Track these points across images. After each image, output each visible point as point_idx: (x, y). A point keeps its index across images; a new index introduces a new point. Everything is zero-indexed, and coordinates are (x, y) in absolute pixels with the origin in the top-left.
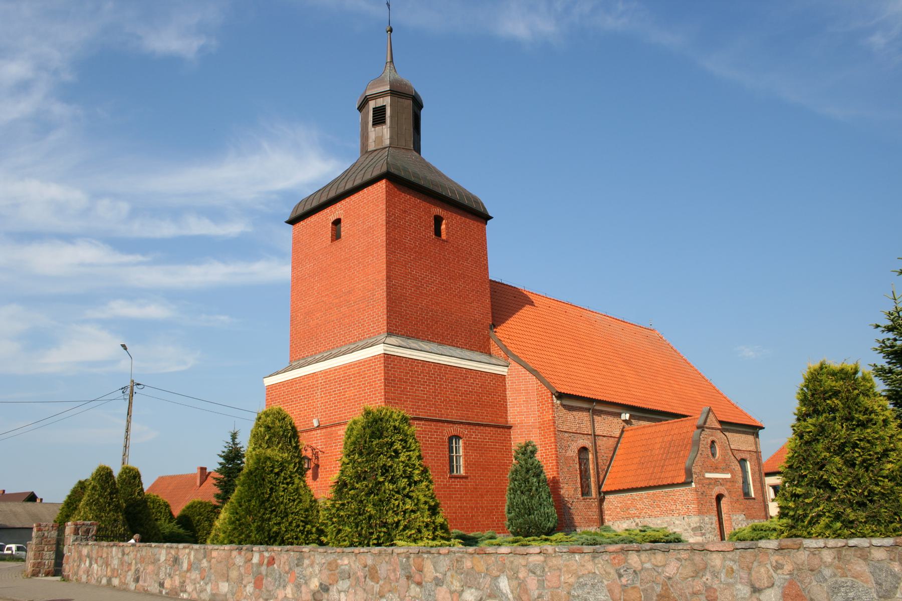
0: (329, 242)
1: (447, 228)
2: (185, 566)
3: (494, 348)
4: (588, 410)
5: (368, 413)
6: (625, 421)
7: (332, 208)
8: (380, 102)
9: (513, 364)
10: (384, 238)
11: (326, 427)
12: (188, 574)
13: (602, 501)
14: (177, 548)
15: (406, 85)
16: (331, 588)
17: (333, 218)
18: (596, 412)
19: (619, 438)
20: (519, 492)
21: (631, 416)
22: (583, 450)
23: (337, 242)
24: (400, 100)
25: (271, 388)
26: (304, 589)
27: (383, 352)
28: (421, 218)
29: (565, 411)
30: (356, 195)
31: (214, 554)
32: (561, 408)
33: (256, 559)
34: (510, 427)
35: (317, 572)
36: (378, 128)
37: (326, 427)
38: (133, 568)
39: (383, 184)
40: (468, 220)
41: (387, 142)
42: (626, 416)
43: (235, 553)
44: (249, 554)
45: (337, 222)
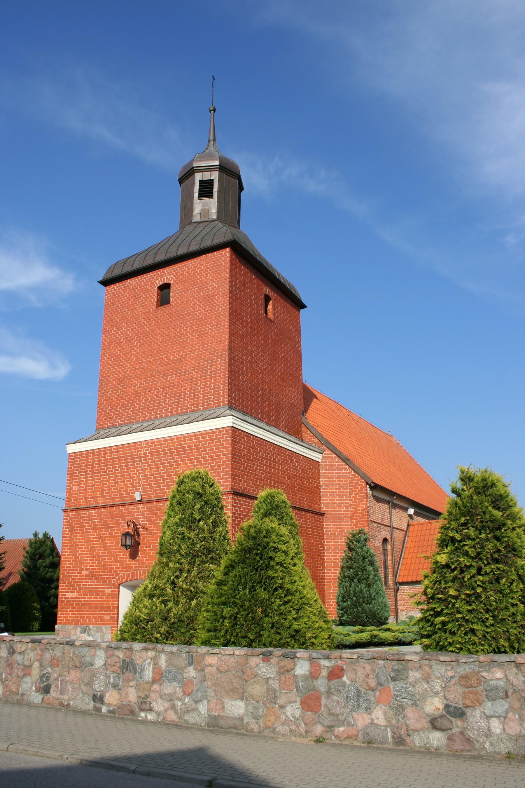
0: (154, 307)
1: (274, 309)
2: (149, 674)
3: (306, 434)
4: (388, 502)
5: (466, 479)
6: (410, 516)
7: (159, 272)
8: (207, 176)
9: (327, 451)
10: (227, 308)
11: (151, 502)
12: (156, 687)
13: (397, 590)
14: (130, 649)
15: (233, 164)
16: (468, 711)
17: (159, 282)
18: (395, 506)
19: (406, 531)
20: (355, 580)
21: (415, 512)
22: (385, 540)
23: (164, 308)
24: (228, 177)
25: (71, 455)
26: (410, 712)
27: (231, 425)
28: (255, 294)
29: (375, 502)
30: (191, 261)
31: (211, 660)
32: (372, 498)
33: (302, 668)
34: (323, 515)
35: (438, 688)
36: (205, 200)
37: (151, 502)
38: (36, 672)
39: (227, 252)
40: (288, 305)
41: (215, 216)
42: (411, 511)
43: (255, 661)
44: (286, 662)
45: (165, 287)
